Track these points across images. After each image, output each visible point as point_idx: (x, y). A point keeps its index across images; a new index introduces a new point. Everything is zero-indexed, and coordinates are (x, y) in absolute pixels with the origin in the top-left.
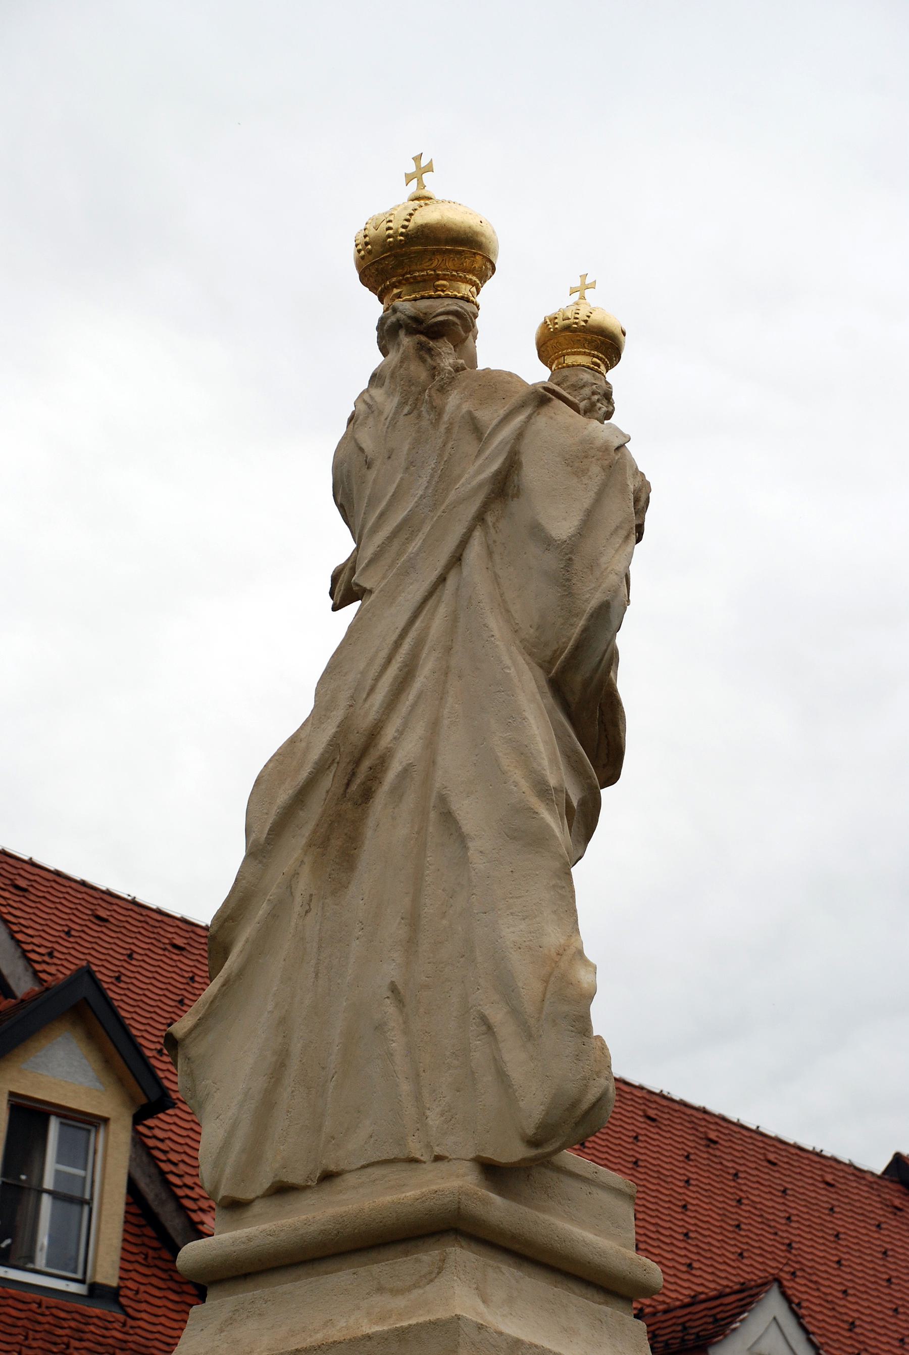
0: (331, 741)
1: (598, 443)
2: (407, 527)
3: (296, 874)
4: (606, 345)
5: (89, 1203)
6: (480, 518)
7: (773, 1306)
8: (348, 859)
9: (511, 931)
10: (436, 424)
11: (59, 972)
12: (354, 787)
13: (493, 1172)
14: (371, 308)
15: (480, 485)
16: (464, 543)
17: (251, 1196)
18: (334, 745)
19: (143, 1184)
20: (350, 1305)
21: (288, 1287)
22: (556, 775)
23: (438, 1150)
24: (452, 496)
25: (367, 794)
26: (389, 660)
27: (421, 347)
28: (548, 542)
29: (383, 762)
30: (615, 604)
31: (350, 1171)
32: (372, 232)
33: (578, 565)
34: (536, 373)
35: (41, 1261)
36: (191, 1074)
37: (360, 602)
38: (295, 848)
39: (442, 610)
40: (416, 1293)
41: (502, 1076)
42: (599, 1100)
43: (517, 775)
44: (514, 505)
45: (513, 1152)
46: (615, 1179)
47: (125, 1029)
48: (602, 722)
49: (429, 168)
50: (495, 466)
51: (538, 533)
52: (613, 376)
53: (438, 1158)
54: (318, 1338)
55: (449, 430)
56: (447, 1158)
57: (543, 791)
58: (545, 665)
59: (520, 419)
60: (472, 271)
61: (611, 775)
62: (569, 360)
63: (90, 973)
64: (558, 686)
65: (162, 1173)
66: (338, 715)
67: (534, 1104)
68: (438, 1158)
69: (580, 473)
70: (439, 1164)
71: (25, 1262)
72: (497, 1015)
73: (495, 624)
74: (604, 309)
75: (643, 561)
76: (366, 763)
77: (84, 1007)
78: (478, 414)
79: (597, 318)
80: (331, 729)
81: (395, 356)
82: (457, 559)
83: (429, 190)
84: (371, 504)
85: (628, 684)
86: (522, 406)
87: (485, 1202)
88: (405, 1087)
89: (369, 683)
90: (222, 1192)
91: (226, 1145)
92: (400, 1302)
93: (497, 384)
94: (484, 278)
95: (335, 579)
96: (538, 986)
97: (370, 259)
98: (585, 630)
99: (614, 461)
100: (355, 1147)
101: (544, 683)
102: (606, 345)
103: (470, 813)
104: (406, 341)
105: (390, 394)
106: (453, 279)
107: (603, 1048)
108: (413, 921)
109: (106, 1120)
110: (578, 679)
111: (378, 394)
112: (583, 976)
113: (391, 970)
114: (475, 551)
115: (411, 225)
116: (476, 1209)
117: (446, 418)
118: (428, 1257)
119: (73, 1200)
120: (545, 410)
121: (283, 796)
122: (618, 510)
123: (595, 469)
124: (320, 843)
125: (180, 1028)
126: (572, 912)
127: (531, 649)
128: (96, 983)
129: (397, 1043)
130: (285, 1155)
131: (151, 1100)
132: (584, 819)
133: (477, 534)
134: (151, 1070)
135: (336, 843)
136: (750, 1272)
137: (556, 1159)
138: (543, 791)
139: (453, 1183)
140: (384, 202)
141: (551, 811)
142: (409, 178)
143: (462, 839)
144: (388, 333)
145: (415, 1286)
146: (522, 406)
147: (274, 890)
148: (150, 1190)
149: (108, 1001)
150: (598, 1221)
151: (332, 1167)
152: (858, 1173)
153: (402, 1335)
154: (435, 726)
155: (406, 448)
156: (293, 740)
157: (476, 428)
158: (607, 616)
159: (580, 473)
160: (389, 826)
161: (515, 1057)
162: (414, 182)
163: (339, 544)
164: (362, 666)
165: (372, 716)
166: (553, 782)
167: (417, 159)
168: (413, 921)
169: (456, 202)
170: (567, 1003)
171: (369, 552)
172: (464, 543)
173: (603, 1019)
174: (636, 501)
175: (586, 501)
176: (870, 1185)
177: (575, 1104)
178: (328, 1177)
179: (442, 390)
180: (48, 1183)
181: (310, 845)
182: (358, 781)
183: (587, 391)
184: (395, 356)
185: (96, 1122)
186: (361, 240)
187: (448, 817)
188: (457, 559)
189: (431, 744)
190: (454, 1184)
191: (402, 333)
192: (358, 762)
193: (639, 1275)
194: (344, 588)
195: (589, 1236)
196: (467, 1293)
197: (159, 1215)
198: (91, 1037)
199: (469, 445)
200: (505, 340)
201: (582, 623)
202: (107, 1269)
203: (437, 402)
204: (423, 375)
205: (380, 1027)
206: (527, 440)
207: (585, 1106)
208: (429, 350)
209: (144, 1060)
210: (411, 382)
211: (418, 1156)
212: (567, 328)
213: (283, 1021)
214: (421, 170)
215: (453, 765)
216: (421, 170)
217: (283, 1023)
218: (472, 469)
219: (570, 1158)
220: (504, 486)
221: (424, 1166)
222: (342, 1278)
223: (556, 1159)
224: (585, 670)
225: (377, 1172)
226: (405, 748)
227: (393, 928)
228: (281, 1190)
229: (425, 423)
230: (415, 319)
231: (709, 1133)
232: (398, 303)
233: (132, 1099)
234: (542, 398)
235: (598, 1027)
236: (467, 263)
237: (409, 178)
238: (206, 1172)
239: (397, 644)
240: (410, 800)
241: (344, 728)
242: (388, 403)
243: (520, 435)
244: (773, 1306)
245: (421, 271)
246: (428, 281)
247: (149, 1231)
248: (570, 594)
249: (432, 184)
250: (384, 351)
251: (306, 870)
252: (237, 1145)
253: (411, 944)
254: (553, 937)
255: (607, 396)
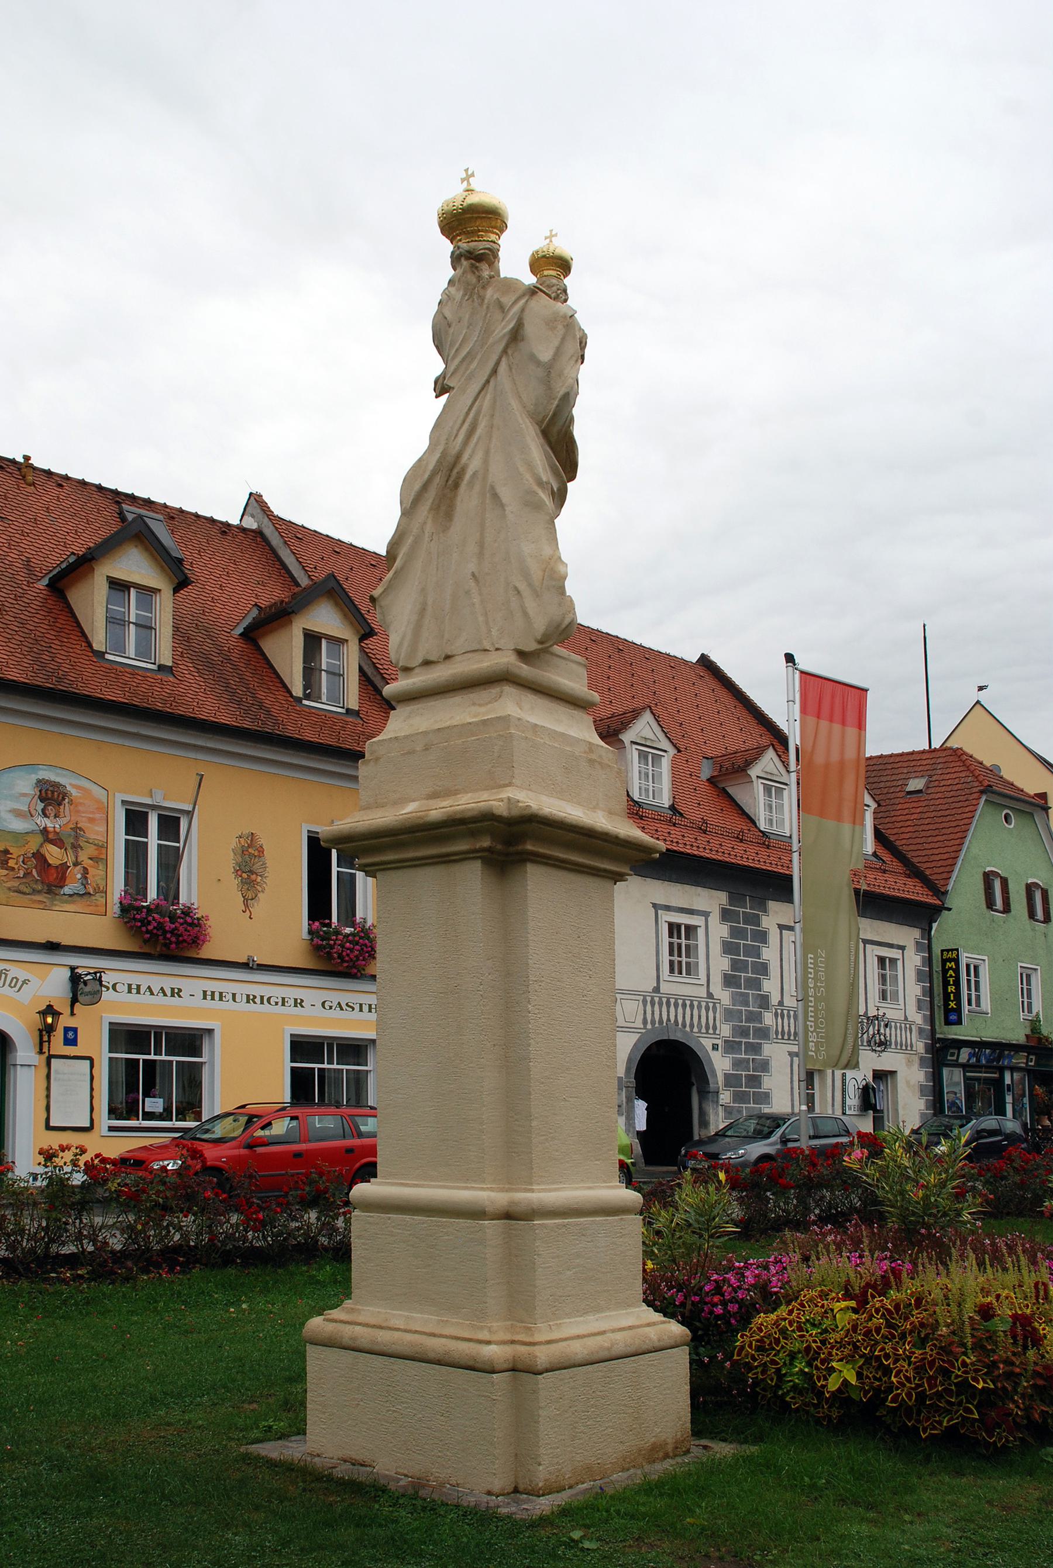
1: (561, 314)
2: (470, 356)
3: (425, 523)
4: (564, 265)
5: (343, 675)
6: (505, 351)
7: (647, 717)
8: (449, 515)
9: (527, 548)
10: (481, 304)
11: (320, 575)
12: (450, 482)
13: (522, 655)
14: (447, 247)
15: (504, 335)
16: (498, 363)
18: (439, 462)
19: (365, 668)
20: (458, 712)
21: (433, 703)
22: (546, 476)
23: (497, 646)
24: (491, 340)
25: (456, 486)
26: (464, 422)
27: (472, 266)
28: (538, 363)
29: (463, 470)
30: (572, 394)
32: (446, 208)
33: (553, 375)
34: (530, 279)
35: (324, 699)
36: (382, 613)
37: (447, 395)
38: (424, 510)
39: (488, 396)
40: (490, 706)
41: (525, 614)
42: (567, 626)
43: (528, 476)
44: (521, 345)
45: (531, 646)
46: (578, 658)
47: (352, 601)
48: (567, 451)
49: (473, 175)
50: (511, 325)
51: (533, 358)
52: (567, 281)
53: (497, 649)
54: (448, 724)
55: (488, 308)
57: (540, 483)
58: (539, 423)
59: (522, 302)
60: (495, 228)
61: (572, 477)
62: (546, 273)
63: (334, 577)
64: (545, 433)
65: (374, 663)
66: (440, 448)
67: (540, 625)
68: (497, 649)
69: (553, 329)
71: (318, 699)
72: (522, 586)
73: (514, 404)
74: (563, 247)
75: (586, 373)
76: (455, 471)
77: (332, 590)
78: (502, 300)
79: (558, 252)
80: (437, 455)
81: (459, 271)
82: (494, 372)
83: (472, 187)
84: (451, 345)
85: (579, 432)
86: (524, 295)
87: (520, 668)
88: (481, 619)
89: (455, 432)
90: (401, 664)
91: (401, 644)
92: (483, 709)
93: (510, 284)
94: (502, 231)
95: (436, 383)
96: (541, 573)
97: (445, 222)
98: (557, 406)
99: (569, 322)
100: (458, 646)
101: (539, 432)
102: (564, 265)
103: (506, 494)
104: (465, 263)
105: (458, 290)
106: (487, 231)
107: (572, 601)
108: (481, 545)
109: (347, 641)
110: (555, 430)
111: (453, 290)
112: (561, 568)
113: (472, 567)
114: (503, 367)
115: (465, 204)
116: (516, 671)
117: (486, 301)
118: (495, 691)
119: (336, 674)
120: (535, 298)
121: (417, 486)
122: (572, 347)
123: (560, 327)
124: (435, 508)
125: (376, 593)
126: (555, 539)
127: (532, 416)
128: (338, 581)
129: (476, 600)
130: (427, 648)
131: (367, 633)
132: (560, 497)
133: (504, 359)
134: (365, 619)
135: (443, 508)
136: (637, 704)
137: (551, 649)
138: (540, 483)
139: (506, 660)
140: (450, 192)
141: (544, 493)
142: (463, 180)
143: (502, 506)
144: (456, 259)
145: (490, 702)
146: (524, 295)
147: (415, 530)
148: (369, 671)
149: (344, 589)
150: (571, 675)
152: (685, 662)
153: (484, 722)
154: (487, 452)
155: (467, 316)
156: (420, 460)
157: (501, 307)
158: (568, 399)
159: (553, 329)
160: (467, 501)
161: (531, 605)
162: (465, 183)
163: (437, 366)
164: (451, 424)
165: (457, 448)
166: (544, 479)
167: (466, 170)
168: (481, 545)
169: (486, 193)
170: (553, 580)
171: (452, 368)
172: (498, 363)
173: (571, 588)
174: (581, 343)
175: (556, 343)
176: (690, 667)
177: (559, 626)
178: (448, 657)
179: (484, 287)
180: (324, 667)
181: (431, 509)
182: (452, 479)
183: (555, 288)
184: (459, 271)
185: (342, 641)
186: (441, 212)
187: (495, 496)
188: (494, 372)
189: (486, 462)
190: (505, 660)
191: (463, 259)
192: (451, 470)
193: (590, 698)
194: (441, 387)
195: (566, 682)
196: (513, 706)
197: (371, 682)
198: (337, 604)
199: (498, 316)
200: (514, 262)
201: (556, 402)
202: (353, 703)
203: (482, 292)
204: (474, 280)
205: (467, 592)
206: (527, 312)
207: (564, 626)
208: (477, 268)
209: (362, 615)
210: (468, 284)
212: (544, 256)
213: (423, 590)
214: (468, 176)
215: (497, 473)
216: (468, 176)
217: (423, 591)
218: (500, 327)
219: (557, 649)
220: (516, 335)
222: (457, 700)
223: (551, 649)
224: (560, 423)
225: (470, 655)
226: (473, 464)
227: (472, 548)
228: (427, 663)
229: (476, 304)
230: (469, 252)
231: (618, 646)
232: (460, 244)
233: (358, 632)
234: (533, 291)
235: (569, 592)
236: (493, 223)
237: (463, 180)
238: (393, 656)
239: (470, 409)
240: (477, 488)
241: (444, 454)
242: (458, 294)
243: (523, 310)
244: (647, 717)
245: (471, 227)
246: (474, 233)
247: (370, 687)
248: (550, 389)
250: (454, 269)
251: (429, 521)
252: (406, 644)
253: (481, 555)
254: (547, 551)
255: (565, 291)
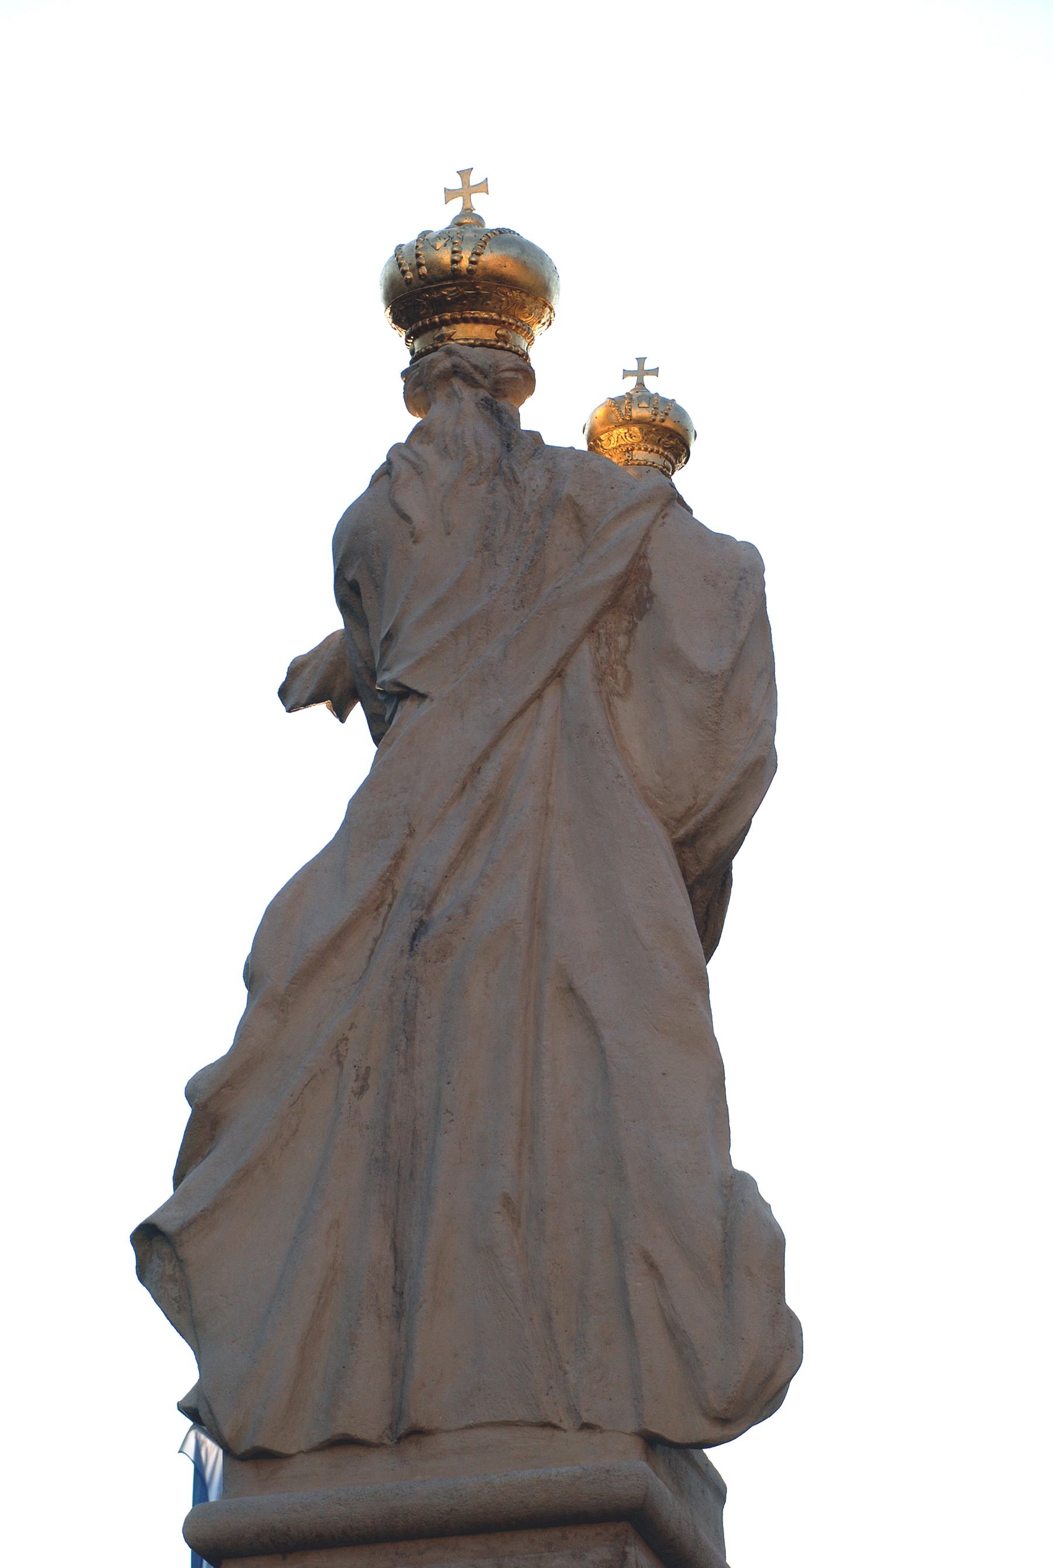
0: (383, 876)
17: (292, 1451)
23: (586, 1417)
28: (691, 673)
31: (448, 1431)
56: (599, 1427)
70: (585, 1435)
133: (586, 647)
142: (450, 195)
151: (423, 1424)
200: (559, 410)
211: (556, 1421)
221: (563, 1434)
245: (461, 305)
249: (480, 204)
